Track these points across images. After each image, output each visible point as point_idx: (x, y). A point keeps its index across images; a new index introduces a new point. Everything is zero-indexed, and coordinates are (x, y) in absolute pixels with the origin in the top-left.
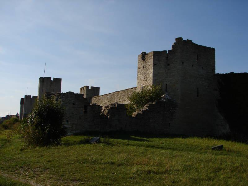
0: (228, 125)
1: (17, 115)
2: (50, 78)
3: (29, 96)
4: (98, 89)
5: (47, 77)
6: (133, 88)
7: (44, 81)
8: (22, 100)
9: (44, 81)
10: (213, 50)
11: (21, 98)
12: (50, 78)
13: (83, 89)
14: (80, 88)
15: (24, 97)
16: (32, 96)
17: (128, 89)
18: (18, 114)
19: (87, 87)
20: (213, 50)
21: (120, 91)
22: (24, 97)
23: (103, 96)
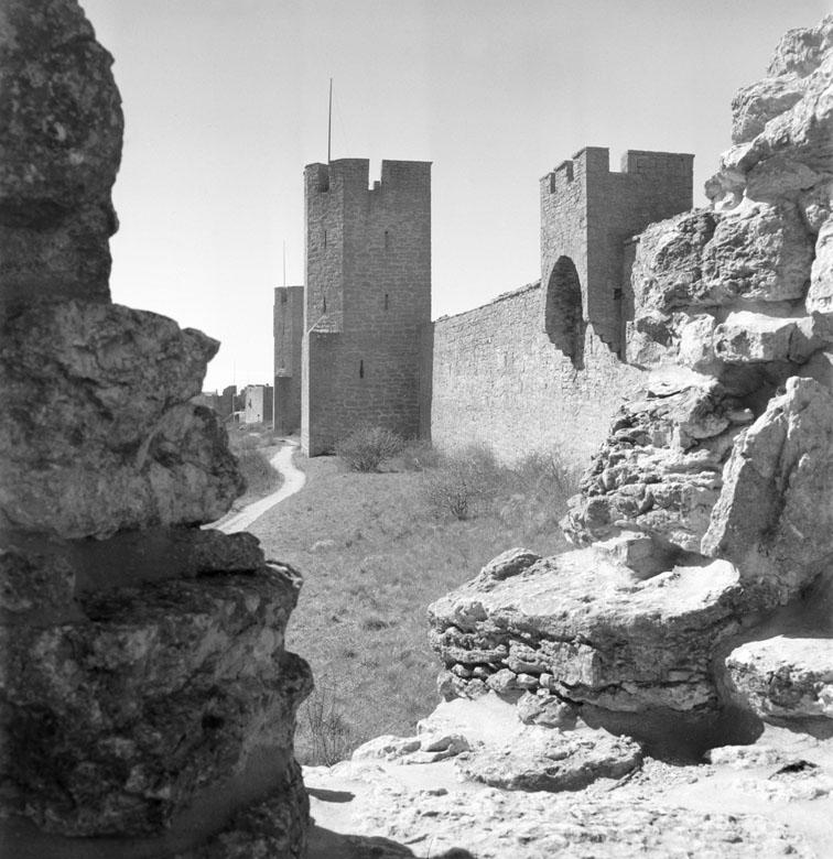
2: (362, 166)
7: (331, 184)
9: (331, 184)
12: (362, 166)
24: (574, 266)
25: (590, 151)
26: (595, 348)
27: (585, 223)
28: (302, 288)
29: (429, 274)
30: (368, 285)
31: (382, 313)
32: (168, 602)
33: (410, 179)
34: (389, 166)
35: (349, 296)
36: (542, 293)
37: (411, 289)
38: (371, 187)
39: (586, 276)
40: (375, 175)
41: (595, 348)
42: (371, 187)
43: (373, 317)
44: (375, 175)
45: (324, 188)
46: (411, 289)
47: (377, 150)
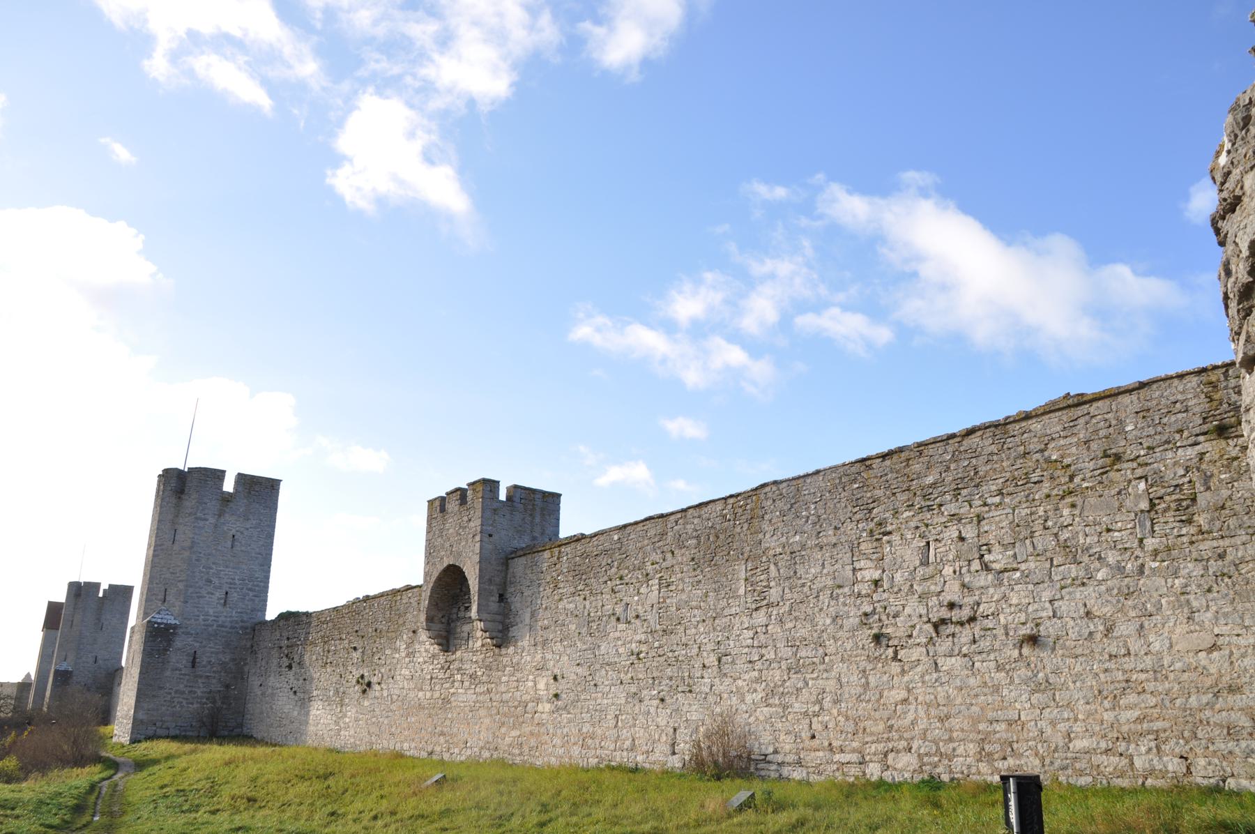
0: (123, 664)
1: (24, 686)
2: (219, 475)
3: (89, 583)
4: (548, 503)
5: (205, 469)
6: (970, 432)
7: (182, 488)
8: (54, 611)
9: (182, 488)
10: (556, 497)
11: (50, 603)
12: (219, 475)
13: (453, 506)
14: (431, 502)
15: (61, 597)
16: (104, 586)
17: (1082, 401)
18: (28, 675)
19: (490, 486)
20: (556, 497)
21: (817, 472)
22: (61, 597)
23: (628, 530)
24: (466, 580)
25: (485, 482)
26: (477, 635)
27: (478, 538)
28: (128, 590)
29: (268, 578)
30: (211, 582)
31: (220, 608)
32: (17, 812)
33: (260, 492)
34: (242, 479)
35: (191, 590)
36: (426, 594)
37: (250, 590)
38: (101, 595)
39: (477, 588)
40: (229, 486)
41: (477, 635)
42: (101, 595)
43: (211, 612)
44: (229, 486)
45: (443, 509)
46: (250, 590)
47: (234, 462)
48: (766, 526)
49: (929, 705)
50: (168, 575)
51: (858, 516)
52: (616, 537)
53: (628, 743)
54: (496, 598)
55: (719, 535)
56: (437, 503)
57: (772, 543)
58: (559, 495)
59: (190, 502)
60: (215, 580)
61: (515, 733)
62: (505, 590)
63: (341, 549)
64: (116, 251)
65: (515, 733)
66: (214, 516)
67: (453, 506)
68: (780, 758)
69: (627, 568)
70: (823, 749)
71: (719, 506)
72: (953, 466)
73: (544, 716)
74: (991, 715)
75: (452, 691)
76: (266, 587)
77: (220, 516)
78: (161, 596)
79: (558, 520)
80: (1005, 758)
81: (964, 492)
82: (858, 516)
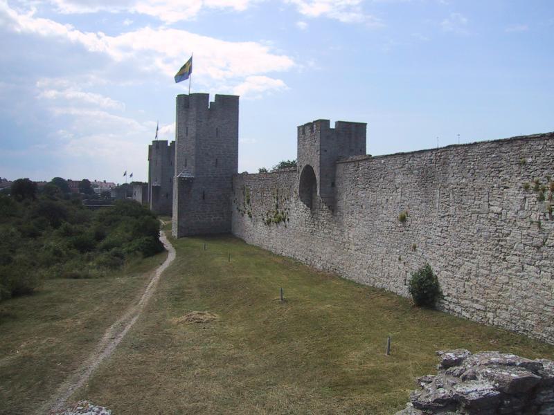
9: (190, 105)
15: (151, 144)
21: (475, 144)
22: (151, 144)
27: (319, 153)
43: (210, 170)
45: (303, 131)
48: (449, 170)
49: (518, 288)
50: (186, 152)
51: (492, 174)
52: (383, 161)
53: (386, 274)
54: (330, 185)
55: (430, 167)
56: (301, 129)
57: (452, 180)
58: (366, 124)
59: (193, 112)
60: (210, 154)
61: (340, 258)
62: (335, 180)
63: (263, 147)
64: (90, 50)
65: (340, 258)
66: (210, 118)
67: (308, 131)
68: (449, 299)
69: (387, 180)
70: (469, 300)
71: (429, 154)
72: (542, 154)
73: (352, 252)
74: (546, 302)
75: (314, 229)
76: (237, 155)
77: (209, 119)
78: (184, 163)
79: (365, 138)
80: (549, 326)
81: (546, 172)
82: (492, 174)
